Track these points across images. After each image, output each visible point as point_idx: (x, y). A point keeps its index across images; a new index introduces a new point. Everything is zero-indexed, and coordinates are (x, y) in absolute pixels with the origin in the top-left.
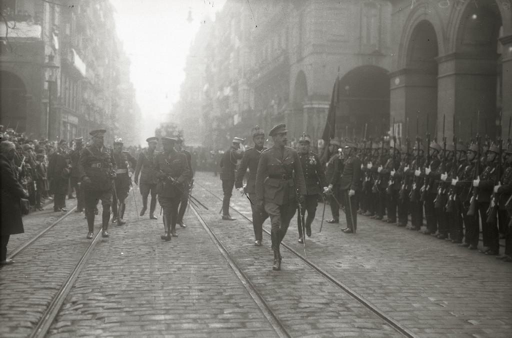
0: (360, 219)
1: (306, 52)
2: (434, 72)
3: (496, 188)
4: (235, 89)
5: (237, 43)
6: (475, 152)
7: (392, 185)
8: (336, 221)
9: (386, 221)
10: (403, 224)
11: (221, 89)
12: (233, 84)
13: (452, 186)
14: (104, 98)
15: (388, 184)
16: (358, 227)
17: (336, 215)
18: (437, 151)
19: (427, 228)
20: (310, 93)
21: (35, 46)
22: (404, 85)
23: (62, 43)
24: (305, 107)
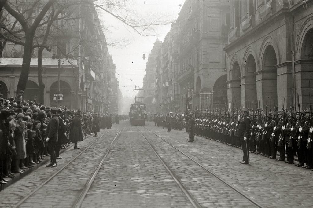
0: (252, 157)
1: (200, 68)
2: (274, 72)
3: (275, 129)
4: (170, 83)
5: (171, 59)
6: (310, 113)
7: (300, 139)
8: (156, 125)
9: (278, 160)
10: (291, 161)
11: (164, 83)
12: (170, 80)
13: (310, 133)
14: (103, 89)
15: (307, 141)
16: (250, 158)
17: (155, 124)
18: (303, 114)
19: (299, 162)
20: (202, 88)
21: (74, 69)
22: (262, 79)
23: (86, 66)
24: (200, 94)
